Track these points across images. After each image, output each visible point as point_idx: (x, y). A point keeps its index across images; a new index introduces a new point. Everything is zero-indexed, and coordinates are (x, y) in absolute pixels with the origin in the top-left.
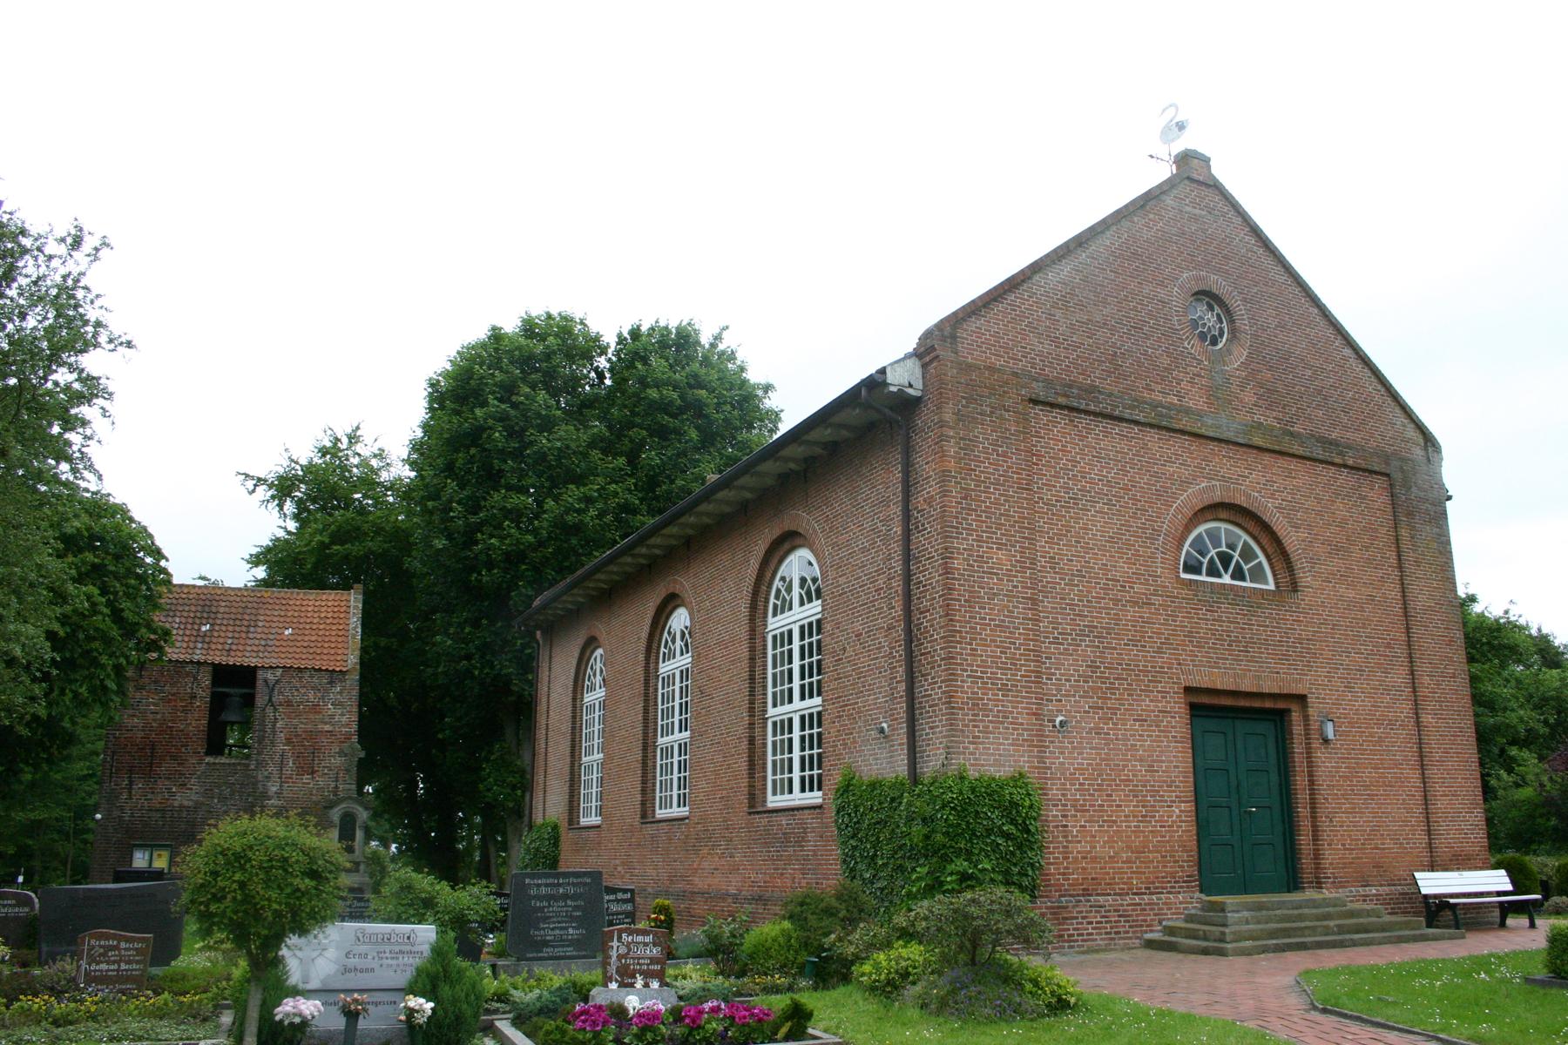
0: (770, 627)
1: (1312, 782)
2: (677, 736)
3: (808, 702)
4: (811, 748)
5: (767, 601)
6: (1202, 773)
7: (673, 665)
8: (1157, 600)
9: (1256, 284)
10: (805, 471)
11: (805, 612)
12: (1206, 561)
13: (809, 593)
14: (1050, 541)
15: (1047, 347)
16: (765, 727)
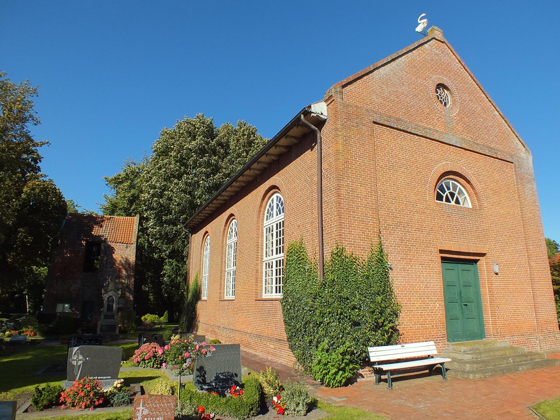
0: (265, 225)
1: (490, 291)
2: (232, 268)
3: (279, 255)
4: (280, 275)
5: (264, 214)
6: (448, 286)
7: (232, 240)
8: (428, 212)
9: (461, 83)
10: (279, 160)
11: (277, 218)
12: (445, 196)
13: (280, 210)
14: (383, 184)
15: (380, 100)
16: (262, 265)
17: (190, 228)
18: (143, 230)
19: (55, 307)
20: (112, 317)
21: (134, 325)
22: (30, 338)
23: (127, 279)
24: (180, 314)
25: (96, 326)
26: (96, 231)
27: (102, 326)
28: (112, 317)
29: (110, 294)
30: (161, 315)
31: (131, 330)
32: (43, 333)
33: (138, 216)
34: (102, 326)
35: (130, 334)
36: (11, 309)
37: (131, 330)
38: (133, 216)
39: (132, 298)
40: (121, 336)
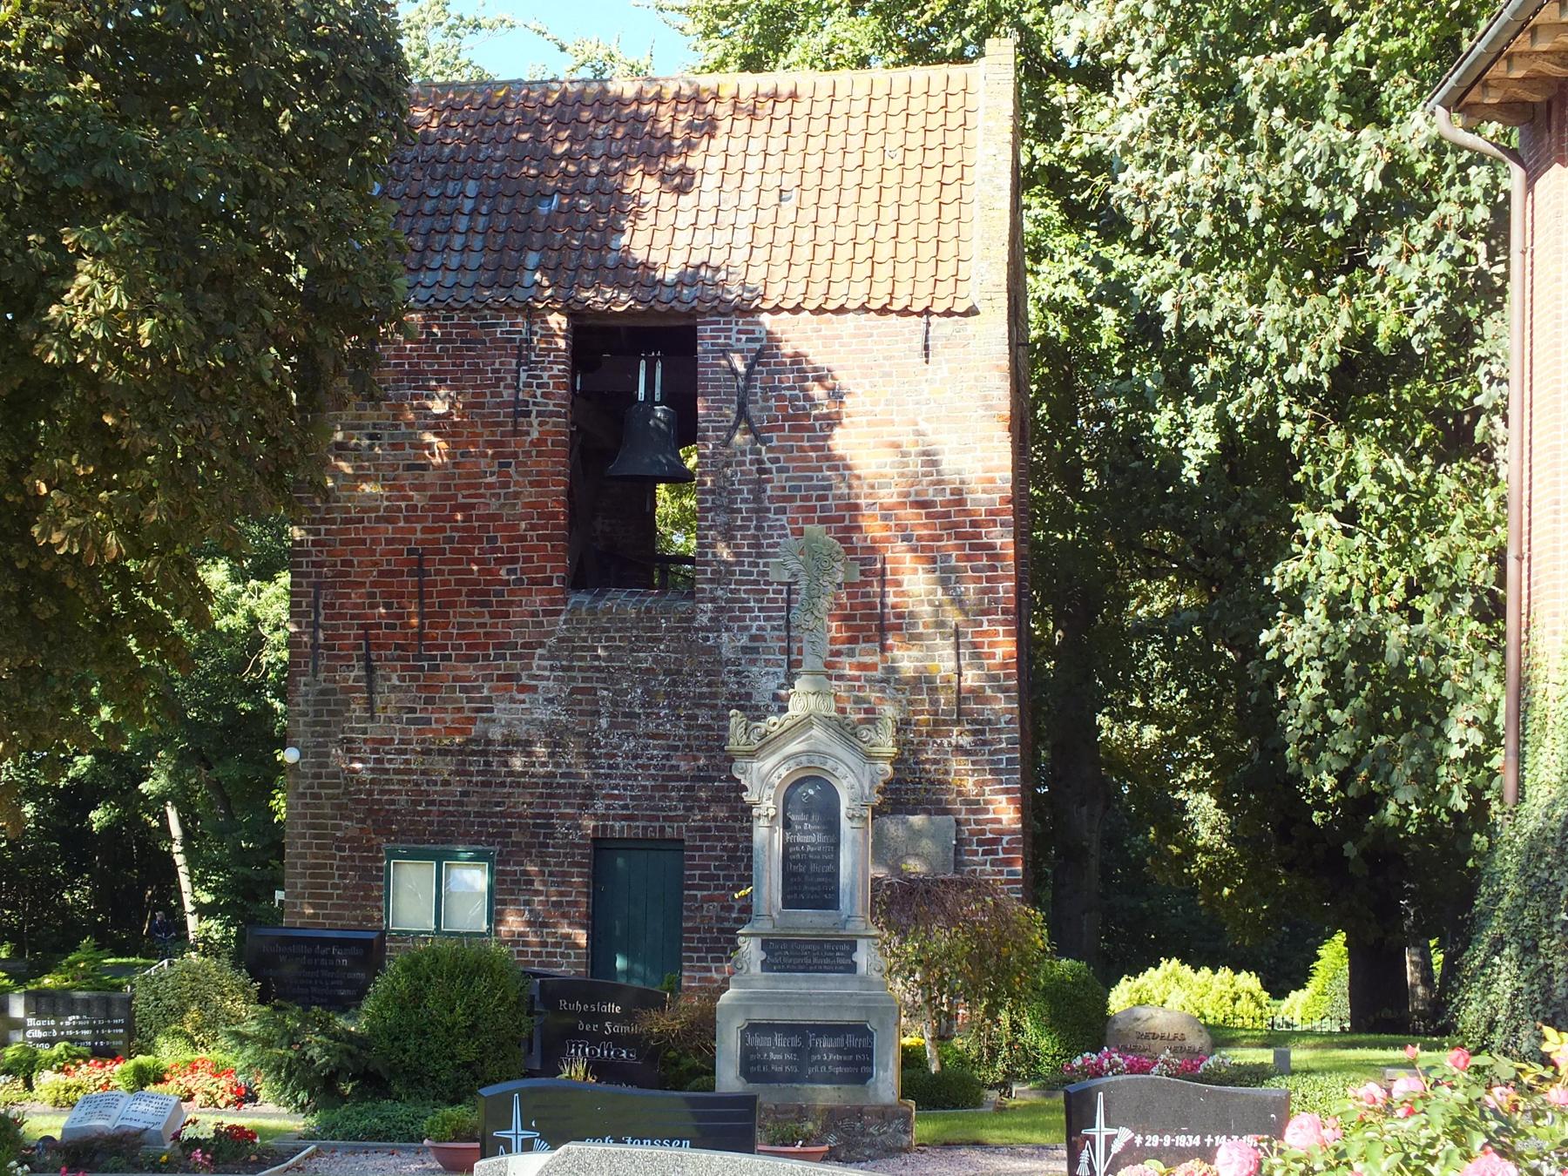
17: (1510, 110)
18: (1066, 190)
19: (372, 886)
20: (833, 955)
21: (1038, 1038)
22: (206, 1122)
23: (955, 643)
24: (1459, 936)
25: (704, 1028)
26: (667, 235)
27: (753, 1028)
28: (833, 955)
29: (795, 745)
30: (1284, 976)
31: (1011, 1076)
32: (314, 1085)
33: (1002, 51)
34: (753, 1028)
35: (1001, 1109)
36: (74, 908)
37: (1011, 1076)
38: (959, 57)
39: (1005, 812)
40: (923, 1129)
